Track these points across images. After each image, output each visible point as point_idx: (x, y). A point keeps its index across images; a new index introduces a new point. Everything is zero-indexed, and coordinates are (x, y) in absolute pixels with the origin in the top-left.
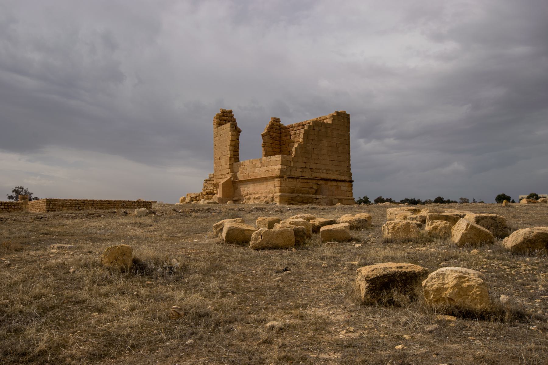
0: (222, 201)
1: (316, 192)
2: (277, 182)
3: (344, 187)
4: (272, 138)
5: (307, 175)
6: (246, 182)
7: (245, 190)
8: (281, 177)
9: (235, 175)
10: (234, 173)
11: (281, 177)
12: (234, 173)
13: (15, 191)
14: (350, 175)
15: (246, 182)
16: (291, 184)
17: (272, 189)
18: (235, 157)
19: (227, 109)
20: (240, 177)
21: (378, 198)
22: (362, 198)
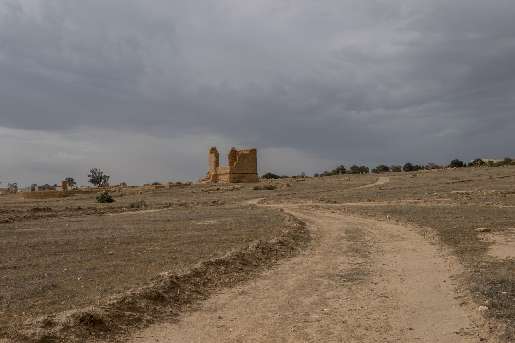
0: (212, 182)
1: (243, 178)
2: (229, 175)
3: (254, 175)
4: (232, 156)
5: (239, 172)
6: (220, 175)
7: (220, 177)
8: (230, 173)
9: (216, 172)
10: (216, 171)
11: (230, 173)
12: (216, 171)
13: (92, 171)
14: (257, 171)
15: (220, 175)
16: (234, 175)
17: (227, 178)
18: (217, 165)
19: (214, 147)
20: (218, 173)
21: (354, 166)
22: (339, 167)
